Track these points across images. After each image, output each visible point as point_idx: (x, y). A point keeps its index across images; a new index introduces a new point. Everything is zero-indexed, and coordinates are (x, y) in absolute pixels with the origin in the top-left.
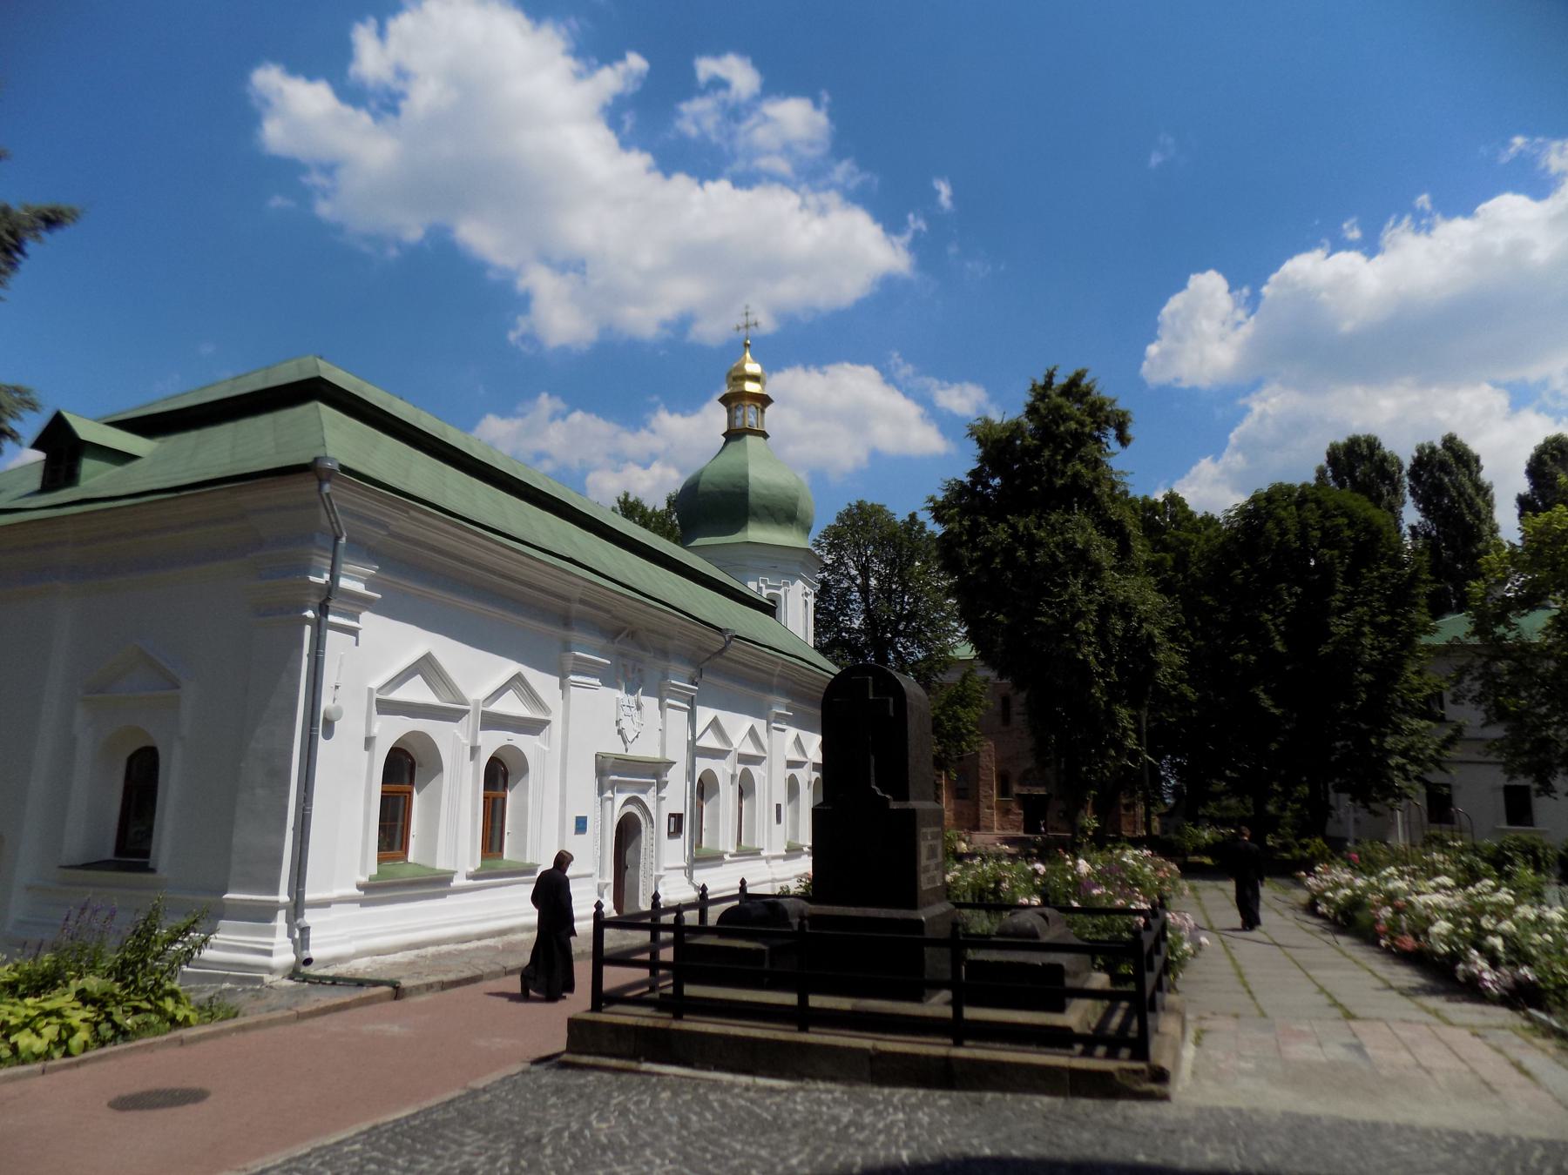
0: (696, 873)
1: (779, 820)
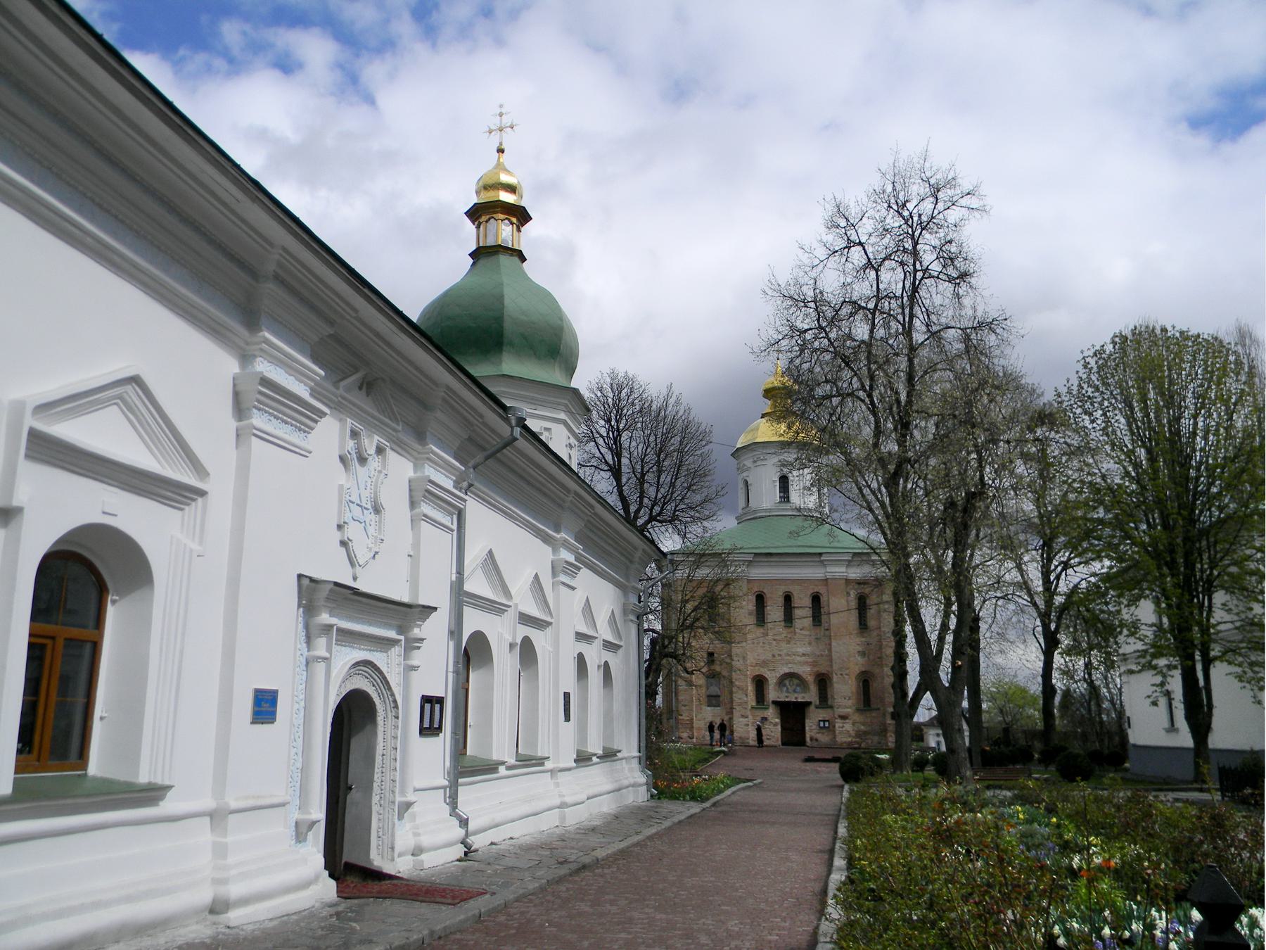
0: (464, 794)
1: (567, 718)
